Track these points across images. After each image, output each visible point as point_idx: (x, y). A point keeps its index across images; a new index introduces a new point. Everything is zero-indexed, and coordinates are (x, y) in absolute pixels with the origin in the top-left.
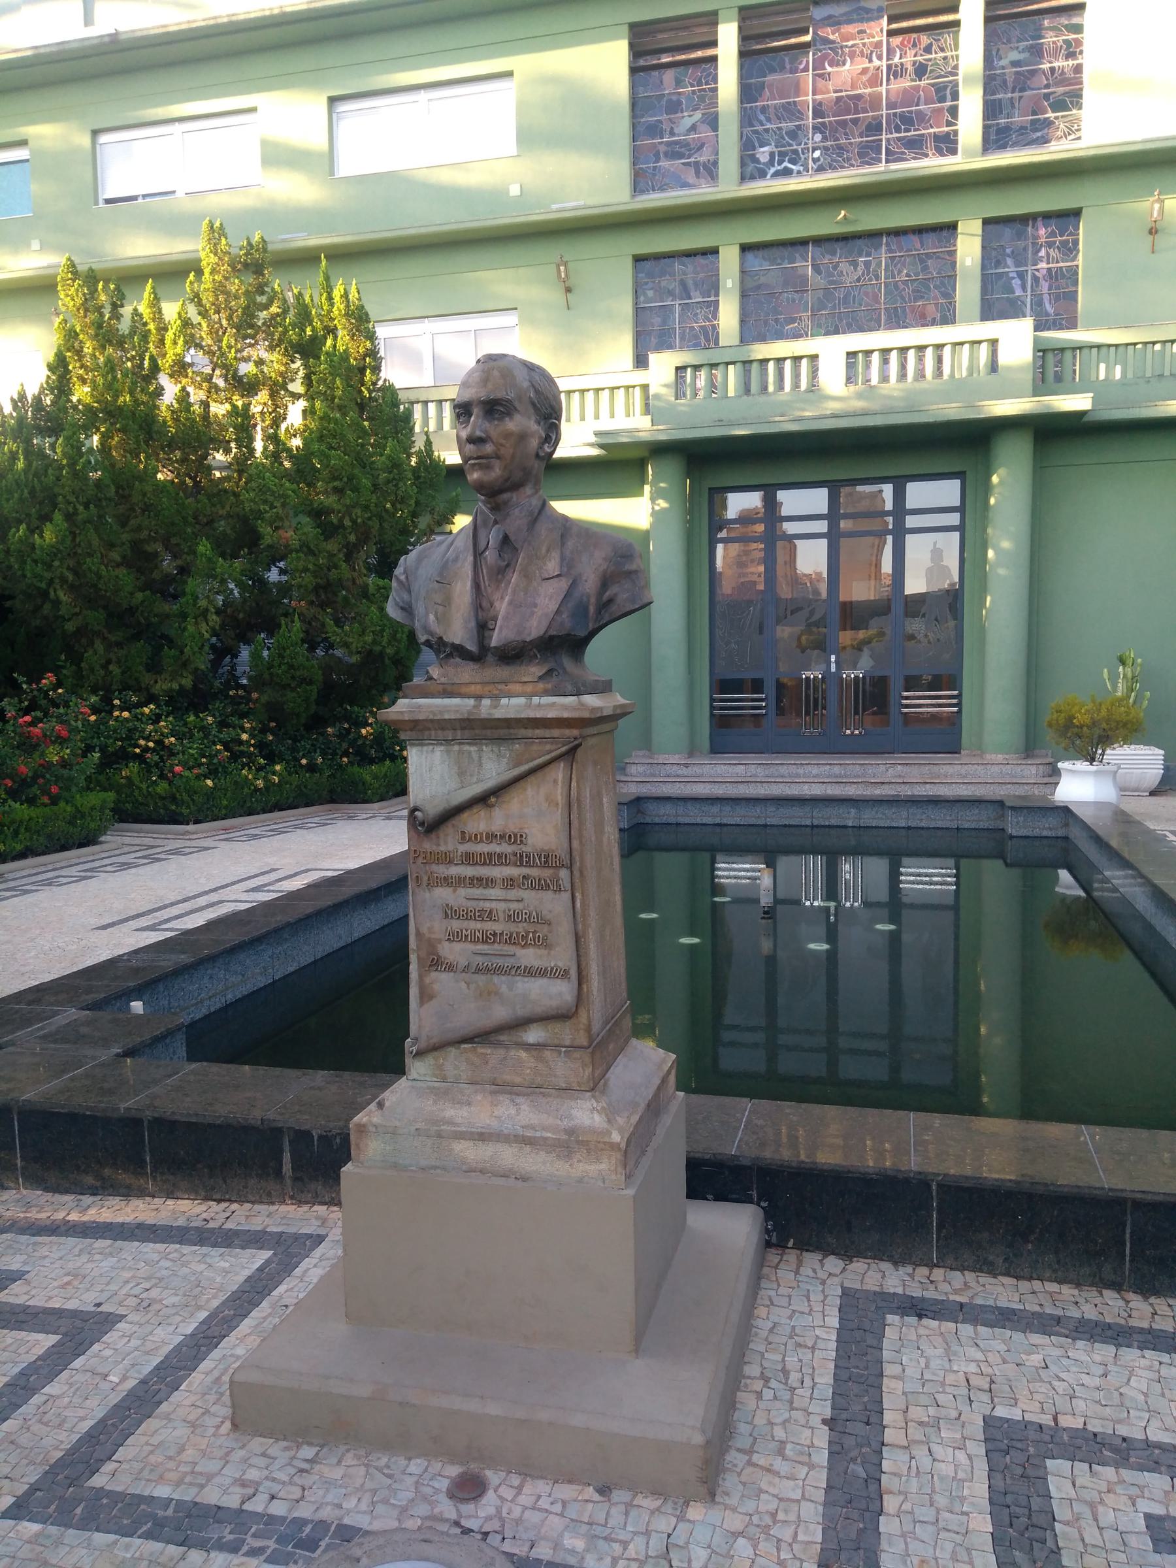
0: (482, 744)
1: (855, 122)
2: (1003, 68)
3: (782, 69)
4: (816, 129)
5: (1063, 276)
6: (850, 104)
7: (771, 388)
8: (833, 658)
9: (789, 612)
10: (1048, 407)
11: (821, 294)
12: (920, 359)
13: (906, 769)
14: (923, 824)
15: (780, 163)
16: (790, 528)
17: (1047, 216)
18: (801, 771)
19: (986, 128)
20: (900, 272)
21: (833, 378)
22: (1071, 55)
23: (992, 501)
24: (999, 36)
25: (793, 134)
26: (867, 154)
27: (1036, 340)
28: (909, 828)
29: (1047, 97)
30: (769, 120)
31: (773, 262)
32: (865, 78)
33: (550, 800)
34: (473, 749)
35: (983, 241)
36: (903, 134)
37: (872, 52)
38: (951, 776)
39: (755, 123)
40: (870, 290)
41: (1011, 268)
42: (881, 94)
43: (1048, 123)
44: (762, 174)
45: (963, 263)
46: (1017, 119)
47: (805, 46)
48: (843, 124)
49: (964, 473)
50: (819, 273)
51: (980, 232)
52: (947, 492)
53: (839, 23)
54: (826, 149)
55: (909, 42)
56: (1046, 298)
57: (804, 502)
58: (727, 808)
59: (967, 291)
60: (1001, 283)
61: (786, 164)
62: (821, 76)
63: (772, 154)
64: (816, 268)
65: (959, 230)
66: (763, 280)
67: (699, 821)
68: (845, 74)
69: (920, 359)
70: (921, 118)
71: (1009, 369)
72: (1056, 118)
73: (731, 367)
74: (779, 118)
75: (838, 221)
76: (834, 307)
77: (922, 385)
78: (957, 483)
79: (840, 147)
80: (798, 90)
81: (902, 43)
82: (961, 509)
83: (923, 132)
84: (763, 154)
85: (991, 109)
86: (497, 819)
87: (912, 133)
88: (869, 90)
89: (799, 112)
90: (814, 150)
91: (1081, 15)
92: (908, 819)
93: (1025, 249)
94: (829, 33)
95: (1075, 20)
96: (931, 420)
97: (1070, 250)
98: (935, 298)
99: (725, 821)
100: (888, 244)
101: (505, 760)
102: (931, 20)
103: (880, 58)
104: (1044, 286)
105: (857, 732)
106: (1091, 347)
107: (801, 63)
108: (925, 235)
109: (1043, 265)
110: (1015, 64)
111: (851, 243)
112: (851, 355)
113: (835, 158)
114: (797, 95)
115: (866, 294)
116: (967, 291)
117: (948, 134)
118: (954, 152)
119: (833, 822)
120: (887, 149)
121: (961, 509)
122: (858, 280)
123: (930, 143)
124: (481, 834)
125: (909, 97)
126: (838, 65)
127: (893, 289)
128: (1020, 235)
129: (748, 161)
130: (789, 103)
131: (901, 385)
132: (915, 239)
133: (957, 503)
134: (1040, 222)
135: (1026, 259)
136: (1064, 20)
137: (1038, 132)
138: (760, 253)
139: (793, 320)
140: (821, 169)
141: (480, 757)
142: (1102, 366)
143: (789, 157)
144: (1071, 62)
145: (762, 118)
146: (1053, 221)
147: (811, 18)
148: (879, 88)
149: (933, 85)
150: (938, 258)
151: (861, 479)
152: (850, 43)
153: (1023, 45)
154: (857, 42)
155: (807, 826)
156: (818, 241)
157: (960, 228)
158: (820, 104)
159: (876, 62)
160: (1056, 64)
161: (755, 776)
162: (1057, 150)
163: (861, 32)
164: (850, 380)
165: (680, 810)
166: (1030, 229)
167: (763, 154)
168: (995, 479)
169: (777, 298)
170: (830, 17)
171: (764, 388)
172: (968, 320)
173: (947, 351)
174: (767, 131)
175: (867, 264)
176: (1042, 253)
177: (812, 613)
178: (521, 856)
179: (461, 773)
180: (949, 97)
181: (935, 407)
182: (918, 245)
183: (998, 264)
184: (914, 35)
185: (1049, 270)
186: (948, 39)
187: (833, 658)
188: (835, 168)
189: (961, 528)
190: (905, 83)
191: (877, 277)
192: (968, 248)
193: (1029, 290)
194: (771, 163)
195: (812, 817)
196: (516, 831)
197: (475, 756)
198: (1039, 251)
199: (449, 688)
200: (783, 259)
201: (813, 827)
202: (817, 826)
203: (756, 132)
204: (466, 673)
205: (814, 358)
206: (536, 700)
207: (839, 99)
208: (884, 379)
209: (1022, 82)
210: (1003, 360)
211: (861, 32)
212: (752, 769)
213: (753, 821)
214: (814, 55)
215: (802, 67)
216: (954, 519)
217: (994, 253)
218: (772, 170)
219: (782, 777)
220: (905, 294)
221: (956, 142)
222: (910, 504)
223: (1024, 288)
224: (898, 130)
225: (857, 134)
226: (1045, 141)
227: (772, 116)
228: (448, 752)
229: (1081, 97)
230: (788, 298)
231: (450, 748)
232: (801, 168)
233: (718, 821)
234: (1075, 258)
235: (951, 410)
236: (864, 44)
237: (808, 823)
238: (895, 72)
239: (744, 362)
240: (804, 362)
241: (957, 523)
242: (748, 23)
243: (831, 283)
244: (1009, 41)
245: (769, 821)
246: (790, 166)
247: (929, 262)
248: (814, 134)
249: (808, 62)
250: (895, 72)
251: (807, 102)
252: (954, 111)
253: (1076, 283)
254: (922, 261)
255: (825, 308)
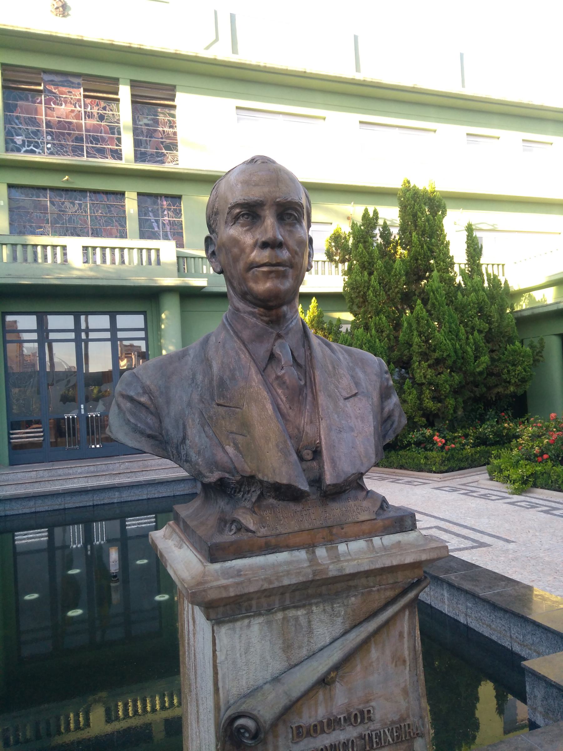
0: (311, 605)
1: (69, 134)
2: (141, 125)
3: (27, 100)
4: (48, 133)
5: (176, 225)
6: (64, 125)
7: (40, 260)
8: (82, 406)
9: (55, 382)
10: (186, 283)
11: (55, 216)
12: (113, 254)
13: (130, 464)
14: (156, 496)
15: (28, 146)
16: (52, 336)
17: (167, 196)
18: (71, 471)
19: (135, 151)
20: (97, 211)
21: (75, 258)
22: (171, 127)
23: (163, 327)
24: (138, 110)
25: (36, 133)
26: (76, 151)
27: (177, 252)
28: (149, 499)
29: (162, 143)
30: (21, 123)
31: (27, 195)
32: (73, 115)
33: (399, 660)
34: (300, 612)
35: (138, 203)
36: (94, 145)
37: (76, 103)
38: (154, 465)
39: (13, 123)
40: (82, 218)
41: (152, 218)
42: (81, 124)
43: (163, 155)
44: (19, 150)
45: (129, 211)
46: (150, 150)
47: (40, 91)
48: (63, 134)
49: (146, 312)
50: (54, 205)
51: (136, 198)
52: (138, 321)
53: (58, 85)
54: (54, 144)
55: (95, 103)
56: (169, 233)
57: (59, 322)
58: (39, 502)
59: (132, 225)
60: (148, 223)
61: (32, 147)
62: (49, 108)
63: (23, 141)
64: (52, 203)
65: (126, 196)
66: (21, 204)
67: (20, 512)
68: (62, 110)
69: (113, 254)
70: (103, 140)
71: (166, 264)
72: (167, 153)
73: (4, 247)
74: (26, 124)
75: (65, 180)
76: (63, 224)
77: (123, 267)
78: (142, 317)
79: (62, 145)
80: (36, 112)
81: (91, 102)
82: (145, 329)
83: (104, 146)
84: (19, 140)
85: (137, 143)
86: (341, 698)
87: (99, 146)
88: (75, 121)
89: (38, 123)
90: (47, 143)
91: (175, 110)
92: (147, 494)
93: (158, 210)
94: (52, 88)
95: (172, 112)
96: (132, 284)
97: (178, 213)
98: (116, 226)
99: (38, 510)
100: (90, 197)
101: (340, 620)
102: (105, 95)
103: (80, 107)
104: (168, 228)
105: (98, 446)
106: (199, 258)
107: (38, 99)
108: (109, 196)
109: (166, 218)
110: (146, 125)
111: (70, 193)
112: (85, 248)
113: (59, 150)
114: (36, 113)
115: (81, 219)
116: (132, 225)
117: (117, 150)
118: (120, 158)
119: (106, 501)
120: (87, 151)
121: (145, 329)
122: (76, 212)
123: (108, 152)
124: (321, 722)
125: (96, 129)
126: (58, 105)
127: (94, 219)
128: (155, 203)
129: (10, 142)
130: (32, 117)
131: (113, 266)
132: (104, 197)
133: (143, 326)
134: (163, 199)
135: (159, 214)
136: (167, 111)
137: (159, 158)
138: (20, 190)
139: (41, 227)
140: (51, 154)
141: (309, 622)
142: (205, 267)
143: (34, 144)
144: (171, 130)
145: (17, 121)
146: (169, 199)
147: (42, 79)
148: (81, 121)
149: (108, 126)
150: (116, 207)
151: (92, 312)
152: (64, 96)
153: (149, 117)
154: (68, 96)
155: (90, 506)
156: (52, 189)
157: (127, 194)
158: (49, 121)
159: (78, 109)
160: (165, 129)
161: (43, 477)
162: (167, 167)
163: (69, 92)
164: (86, 262)
165: (8, 507)
166: (159, 201)
167: (19, 140)
168: (163, 316)
169: (31, 215)
170: (52, 81)
171: (36, 260)
172: (132, 238)
173: (126, 251)
174: (20, 129)
175: (80, 205)
176: (166, 213)
177: (69, 382)
178: (370, 737)
179: (287, 647)
180: (116, 133)
181: (134, 278)
182: (106, 200)
183: (145, 215)
184: (97, 100)
185: (169, 221)
186: (114, 106)
187: (82, 406)
188: (59, 155)
189: (146, 339)
190: (94, 122)
191: (86, 212)
192: (131, 205)
193: (161, 228)
194: (23, 145)
195: (93, 500)
196: (361, 707)
197: (303, 621)
198: (164, 211)
199: (273, 541)
200: (33, 195)
201: (94, 506)
202: (97, 505)
203: (13, 128)
204: (290, 519)
205: (64, 248)
206: (377, 541)
207: (59, 122)
208: (104, 261)
209: (151, 134)
210: (162, 260)
211: (69, 92)
212: (41, 473)
213: (57, 507)
214: (45, 97)
215: (38, 101)
216: (142, 334)
217: (143, 210)
218: (24, 149)
219: (60, 476)
220: (101, 222)
221: (121, 154)
222: (119, 326)
223: (159, 227)
224: (92, 143)
225: (70, 140)
226: (163, 162)
227: (23, 121)
228: (269, 623)
229: (177, 146)
230: (37, 215)
231: (270, 617)
232: (41, 151)
233: (33, 510)
234: (180, 217)
235: (141, 280)
236: (71, 98)
237: (91, 504)
238: (89, 115)
239: (12, 244)
240: (58, 248)
241: (144, 336)
242: (6, 72)
243: (60, 211)
244: (143, 114)
245: (67, 506)
246: (34, 149)
247: (112, 209)
248: (47, 136)
249: (41, 100)
250: (89, 115)
251: (42, 119)
252: (119, 140)
253: (182, 229)
254: (108, 208)
255: (58, 223)
